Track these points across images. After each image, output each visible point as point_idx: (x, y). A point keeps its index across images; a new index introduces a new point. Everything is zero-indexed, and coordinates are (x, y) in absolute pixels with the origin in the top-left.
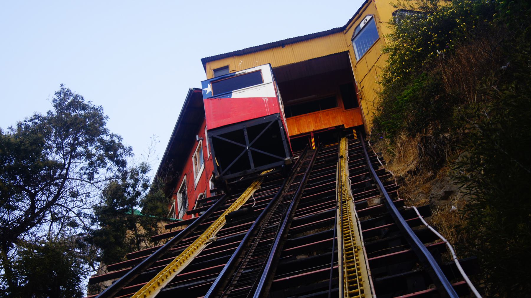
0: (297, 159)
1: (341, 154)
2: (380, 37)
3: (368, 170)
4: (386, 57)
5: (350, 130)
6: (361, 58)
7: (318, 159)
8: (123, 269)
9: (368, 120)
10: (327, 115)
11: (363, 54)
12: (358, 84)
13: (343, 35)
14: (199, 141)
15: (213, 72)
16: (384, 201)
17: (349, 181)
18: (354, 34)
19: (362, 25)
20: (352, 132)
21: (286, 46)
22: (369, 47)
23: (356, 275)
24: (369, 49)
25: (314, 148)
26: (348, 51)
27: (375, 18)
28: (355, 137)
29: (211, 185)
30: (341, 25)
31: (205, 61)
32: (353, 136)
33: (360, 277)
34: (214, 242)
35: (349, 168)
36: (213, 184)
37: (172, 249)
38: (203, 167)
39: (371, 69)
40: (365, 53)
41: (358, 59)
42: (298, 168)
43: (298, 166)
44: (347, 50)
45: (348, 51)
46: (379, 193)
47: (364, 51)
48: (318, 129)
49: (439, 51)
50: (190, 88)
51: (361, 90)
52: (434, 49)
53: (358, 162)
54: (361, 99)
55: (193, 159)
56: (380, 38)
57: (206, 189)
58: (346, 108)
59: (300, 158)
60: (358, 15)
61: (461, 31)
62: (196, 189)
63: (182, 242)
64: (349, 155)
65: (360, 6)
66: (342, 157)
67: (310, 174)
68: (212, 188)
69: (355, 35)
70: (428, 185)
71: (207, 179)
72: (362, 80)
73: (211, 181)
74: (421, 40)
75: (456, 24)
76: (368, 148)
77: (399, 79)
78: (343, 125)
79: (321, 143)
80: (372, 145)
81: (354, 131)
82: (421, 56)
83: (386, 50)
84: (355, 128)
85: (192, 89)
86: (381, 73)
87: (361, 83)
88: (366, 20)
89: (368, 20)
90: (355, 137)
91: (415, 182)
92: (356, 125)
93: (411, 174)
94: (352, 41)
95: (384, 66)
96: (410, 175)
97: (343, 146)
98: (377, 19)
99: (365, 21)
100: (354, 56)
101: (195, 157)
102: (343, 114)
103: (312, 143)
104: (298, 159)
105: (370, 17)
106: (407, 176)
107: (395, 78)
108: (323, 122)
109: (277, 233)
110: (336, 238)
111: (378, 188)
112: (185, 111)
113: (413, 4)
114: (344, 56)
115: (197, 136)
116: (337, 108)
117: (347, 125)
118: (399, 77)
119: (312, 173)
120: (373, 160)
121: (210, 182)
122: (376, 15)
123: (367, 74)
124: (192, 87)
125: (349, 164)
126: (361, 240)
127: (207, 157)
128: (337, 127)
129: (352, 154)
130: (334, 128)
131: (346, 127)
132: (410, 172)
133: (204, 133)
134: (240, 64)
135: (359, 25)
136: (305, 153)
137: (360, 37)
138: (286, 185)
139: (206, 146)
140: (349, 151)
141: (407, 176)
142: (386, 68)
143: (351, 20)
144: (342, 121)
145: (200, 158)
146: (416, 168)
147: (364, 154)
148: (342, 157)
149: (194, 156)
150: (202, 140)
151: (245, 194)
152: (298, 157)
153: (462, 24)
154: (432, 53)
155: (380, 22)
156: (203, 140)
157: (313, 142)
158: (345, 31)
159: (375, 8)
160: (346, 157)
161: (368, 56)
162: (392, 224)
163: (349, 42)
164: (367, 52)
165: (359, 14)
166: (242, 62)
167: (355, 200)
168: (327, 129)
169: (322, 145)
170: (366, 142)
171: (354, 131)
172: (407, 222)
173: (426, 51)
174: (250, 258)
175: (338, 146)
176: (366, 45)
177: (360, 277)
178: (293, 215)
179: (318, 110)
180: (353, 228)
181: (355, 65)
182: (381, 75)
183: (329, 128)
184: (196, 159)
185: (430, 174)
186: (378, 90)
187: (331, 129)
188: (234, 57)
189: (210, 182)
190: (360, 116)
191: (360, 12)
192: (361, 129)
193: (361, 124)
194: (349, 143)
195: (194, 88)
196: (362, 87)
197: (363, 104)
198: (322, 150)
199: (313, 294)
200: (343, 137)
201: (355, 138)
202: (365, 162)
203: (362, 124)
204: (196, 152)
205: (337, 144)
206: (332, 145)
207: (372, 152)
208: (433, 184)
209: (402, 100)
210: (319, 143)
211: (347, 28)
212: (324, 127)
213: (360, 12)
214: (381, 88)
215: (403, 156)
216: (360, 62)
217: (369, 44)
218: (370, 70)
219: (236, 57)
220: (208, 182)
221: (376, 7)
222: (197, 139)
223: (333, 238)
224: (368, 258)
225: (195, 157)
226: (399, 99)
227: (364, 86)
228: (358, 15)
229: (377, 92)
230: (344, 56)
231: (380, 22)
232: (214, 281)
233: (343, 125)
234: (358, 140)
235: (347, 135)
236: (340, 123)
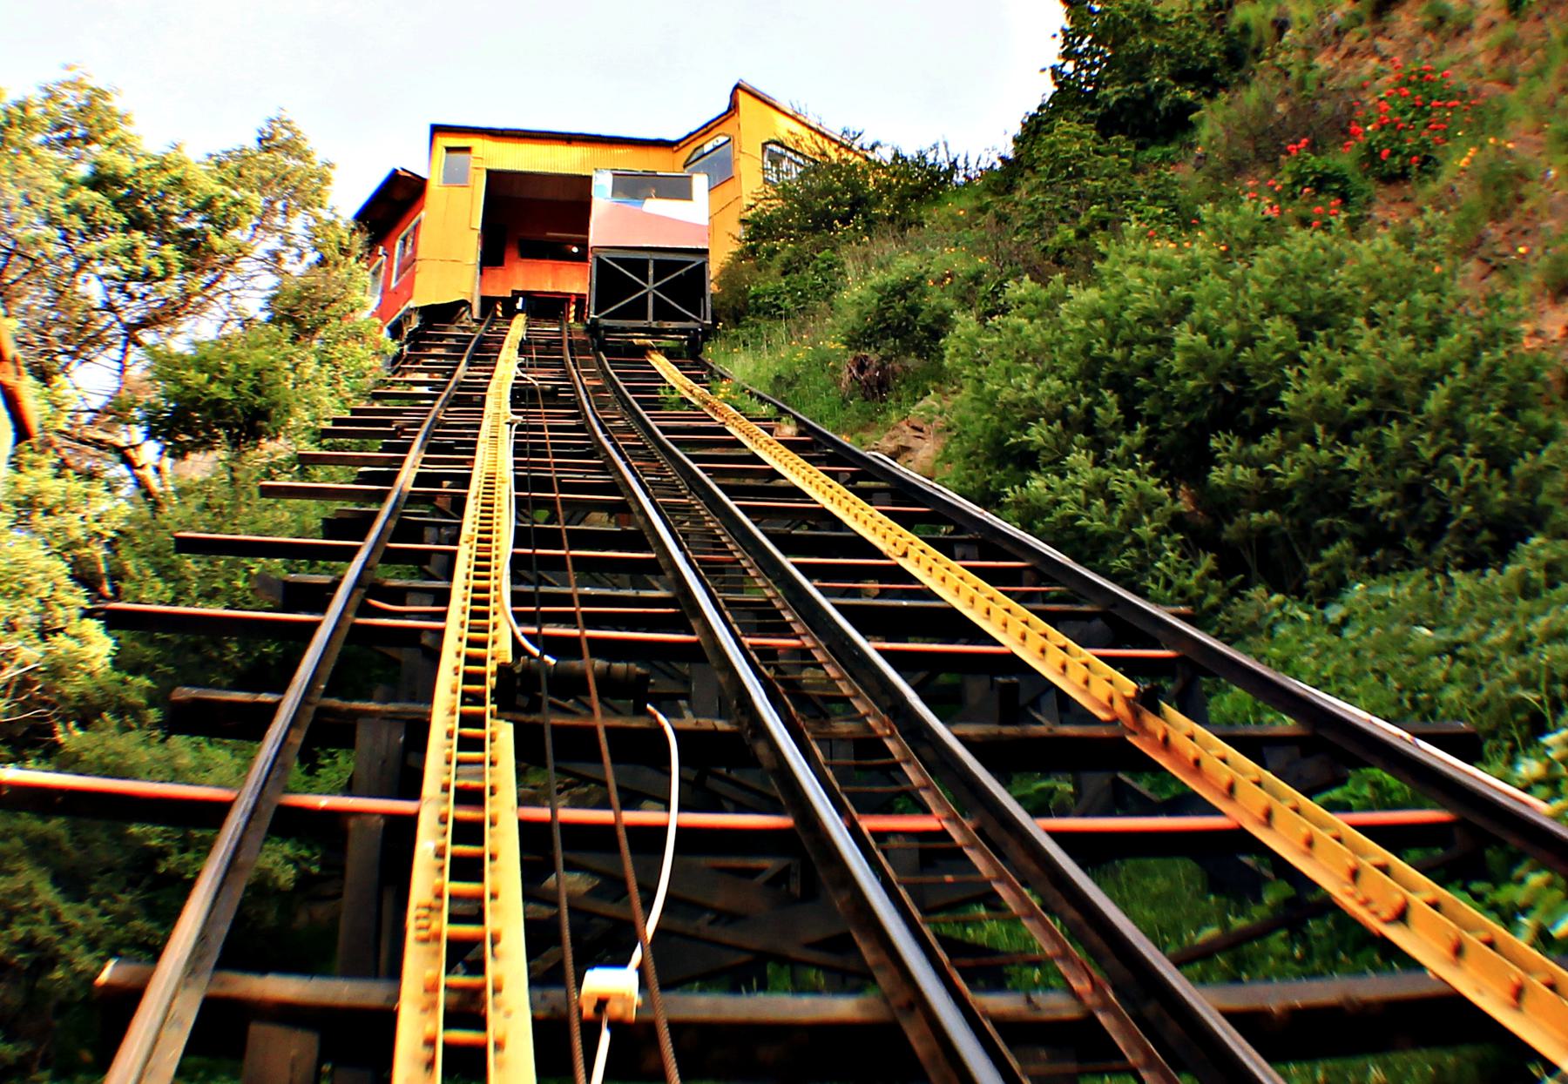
19: (707, 148)
31: (437, 130)
135: (702, 146)
137: (702, 164)
143: (691, 135)
156: (389, 256)
165: (707, 129)
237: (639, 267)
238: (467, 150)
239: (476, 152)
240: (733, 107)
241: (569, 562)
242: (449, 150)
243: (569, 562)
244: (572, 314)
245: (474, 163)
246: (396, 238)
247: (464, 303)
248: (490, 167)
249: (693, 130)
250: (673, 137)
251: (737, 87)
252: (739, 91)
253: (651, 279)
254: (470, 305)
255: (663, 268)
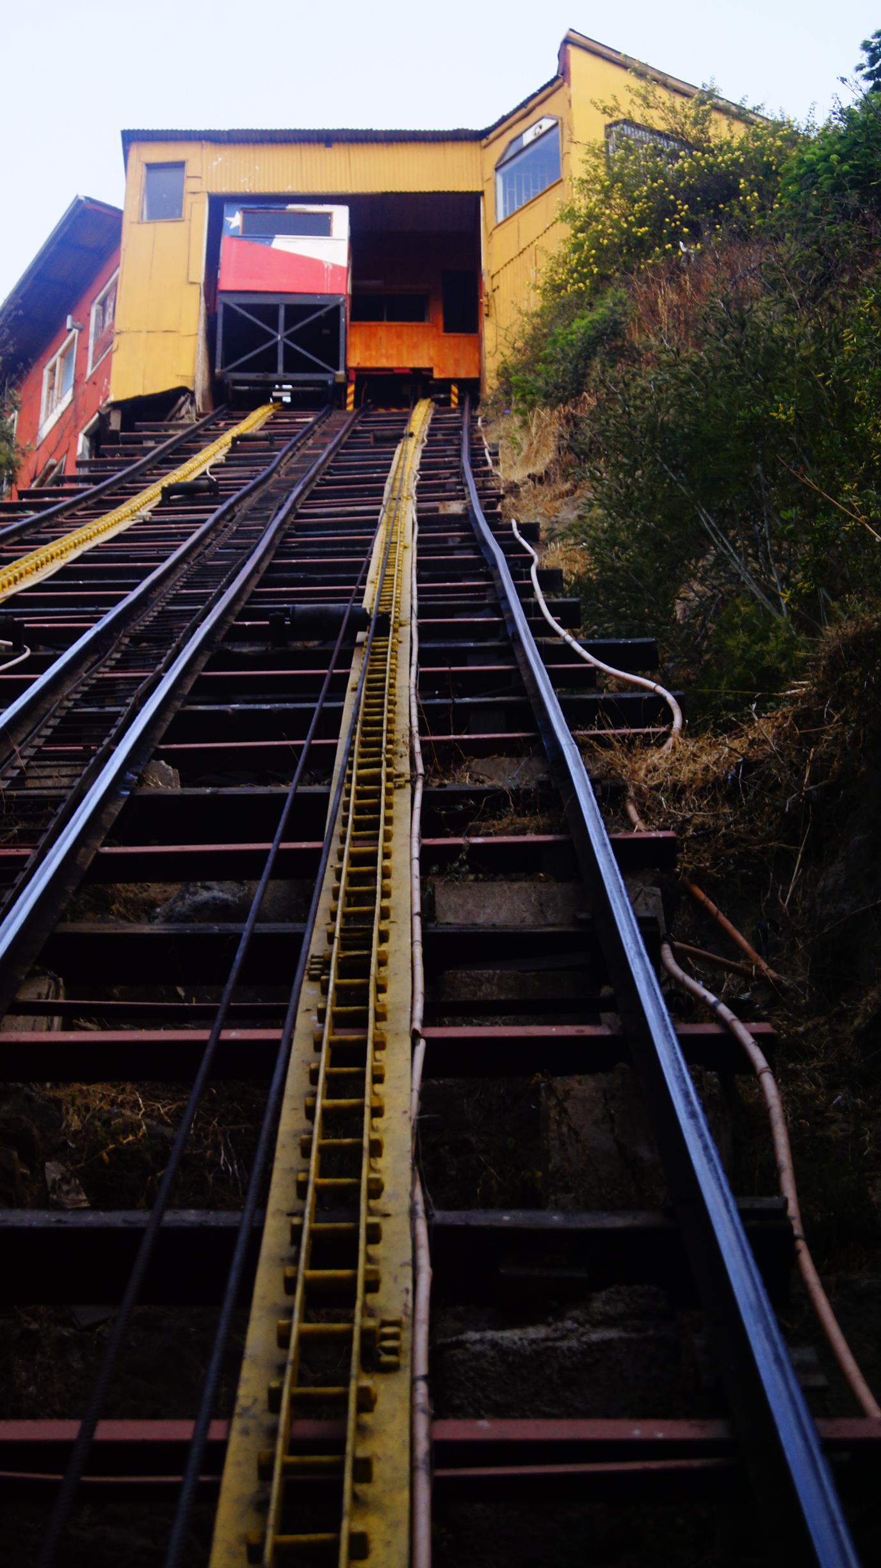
0: (307, 423)
1: (412, 430)
2: (563, 177)
3: (460, 466)
4: (565, 230)
5: (445, 384)
6: (508, 215)
7: (355, 432)
8: (47, 499)
9: (491, 365)
10: (399, 336)
11: (517, 207)
12: (486, 279)
13: (478, 150)
14: (70, 330)
15: (145, 168)
16: (469, 509)
17: (416, 477)
18: (503, 155)
19: (528, 137)
20: (449, 391)
21: (336, 147)
22: (534, 193)
23: (382, 721)
24: (532, 198)
25: (350, 408)
26: (482, 193)
27: (562, 127)
28: (454, 403)
29: (82, 445)
30: (480, 127)
31: (131, 138)
32: (448, 401)
33: (390, 813)
34: (145, 523)
35: (422, 458)
36: (87, 443)
37: (60, 520)
38: (68, 397)
39: (525, 249)
40: (521, 207)
41: (501, 218)
42: (308, 439)
43: (308, 435)
44: (480, 189)
45: (482, 193)
46: (464, 499)
47: (520, 202)
48: (368, 364)
49: (685, 246)
50: (77, 196)
51: (490, 293)
52: (675, 236)
53: (445, 451)
54: (487, 315)
55: (46, 373)
56: (561, 181)
57: (67, 452)
58: (448, 329)
59: (315, 423)
60: (523, 111)
61: (744, 208)
62: (41, 449)
63: (73, 514)
64: (429, 435)
65: (535, 90)
66: (411, 435)
67: (335, 454)
68: (83, 454)
69: (507, 157)
70: (557, 504)
71: (76, 428)
72: (498, 272)
73: (85, 434)
74: (646, 208)
75: (735, 192)
76: (473, 430)
77: (580, 288)
78: (431, 370)
79: (369, 401)
80: (483, 426)
81: (454, 389)
82: (640, 247)
83: (570, 215)
84: (460, 383)
85: (83, 199)
86: (544, 265)
87: (495, 278)
88: (541, 127)
89: (545, 128)
90: (454, 403)
91: (535, 496)
92: (462, 375)
93: (534, 480)
94: (497, 169)
95: (554, 251)
96: (531, 483)
97: (421, 416)
98: (566, 132)
99: (538, 129)
100: (492, 211)
101: (53, 370)
102: (436, 343)
103: (346, 396)
104: (309, 425)
105: (552, 122)
106: (525, 483)
107: (573, 284)
108: (383, 351)
109: (124, 710)
110: (361, 587)
111: (466, 492)
112: (52, 249)
113: (652, 117)
114: (469, 203)
115: (69, 318)
116: (427, 323)
117: (442, 371)
118: (581, 285)
119: (339, 454)
120: (476, 455)
121: (81, 437)
122: (565, 121)
123: (548, 228)
124: (84, 192)
125: (424, 452)
126: (410, 665)
127: (83, 374)
128: (416, 371)
129: (436, 435)
130: (407, 371)
131: (437, 375)
132: (531, 477)
133: (89, 315)
134: (215, 163)
135: (521, 135)
136: (328, 414)
137: (519, 165)
138: (282, 464)
139: (87, 348)
140: (431, 429)
141: (525, 483)
142: (559, 256)
143: (504, 119)
144: (431, 359)
145: (65, 373)
146: (546, 472)
147: (461, 439)
148: (411, 435)
149: (50, 365)
150: (81, 331)
151: (55, 548)
152: (310, 420)
153: (751, 195)
154: (670, 245)
155: (571, 141)
156: (83, 330)
157: (351, 394)
158: (484, 142)
159: (567, 103)
160: (420, 439)
161: (523, 217)
162: (558, 837)
163: (489, 170)
164: (527, 205)
165: (526, 109)
166: (220, 159)
167: (418, 501)
168: (391, 369)
169: (371, 407)
170: (474, 419)
171: (454, 389)
172: (549, 671)
173: (656, 236)
174: (39, 747)
175: (409, 414)
176: (527, 190)
177: (390, 813)
178: (299, 506)
179: (379, 318)
180: (394, 695)
181: (490, 230)
182: (544, 269)
183: (397, 368)
184: (54, 375)
185: (567, 486)
186: (524, 306)
187: (401, 371)
188: (204, 142)
189: (81, 437)
190: (477, 355)
191: (530, 105)
192: (471, 388)
193: (474, 375)
194: (436, 412)
195: (87, 198)
196: (494, 287)
197: (489, 331)
198: (369, 416)
199: (288, 705)
200: (425, 397)
201: (453, 406)
202: (458, 454)
203: (477, 376)
204: (56, 358)
205: (405, 410)
206: (394, 410)
207: (480, 439)
208: (566, 504)
209: (566, 338)
210: (365, 401)
211: (492, 136)
212: (384, 363)
213: (530, 105)
214: (535, 302)
215: (536, 453)
216: (505, 224)
217: (535, 187)
218: (522, 252)
219: (208, 144)
220: (77, 437)
221: (570, 101)
222: (69, 326)
223: (353, 587)
224: (418, 582)
225: (53, 370)
226: (560, 334)
227: (501, 287)
228: (523, 111)
229: (520, 311)
230: (469, 203)
231: (571, 141)
232: (106, 612)
233: (431, 370)
234: (458, 411)
235: (436, 396)
236: (422, 363)
237: (268, 313)
238: (180, 165)
239: (190, 170)
240: (564, 73)
241: (317, 788)
242: (151, 167)
243: (317, 788)
244: (350, 399)
245: (190, 185)
246: (92, 302)
247: (182, 391)
248: (210, 191)
249: (506, 113)
250: (479, 126)
251: (567, 42)
252: (570, 47)
253: (274, 333)
254: (192, 393)
255: (296, 312)
